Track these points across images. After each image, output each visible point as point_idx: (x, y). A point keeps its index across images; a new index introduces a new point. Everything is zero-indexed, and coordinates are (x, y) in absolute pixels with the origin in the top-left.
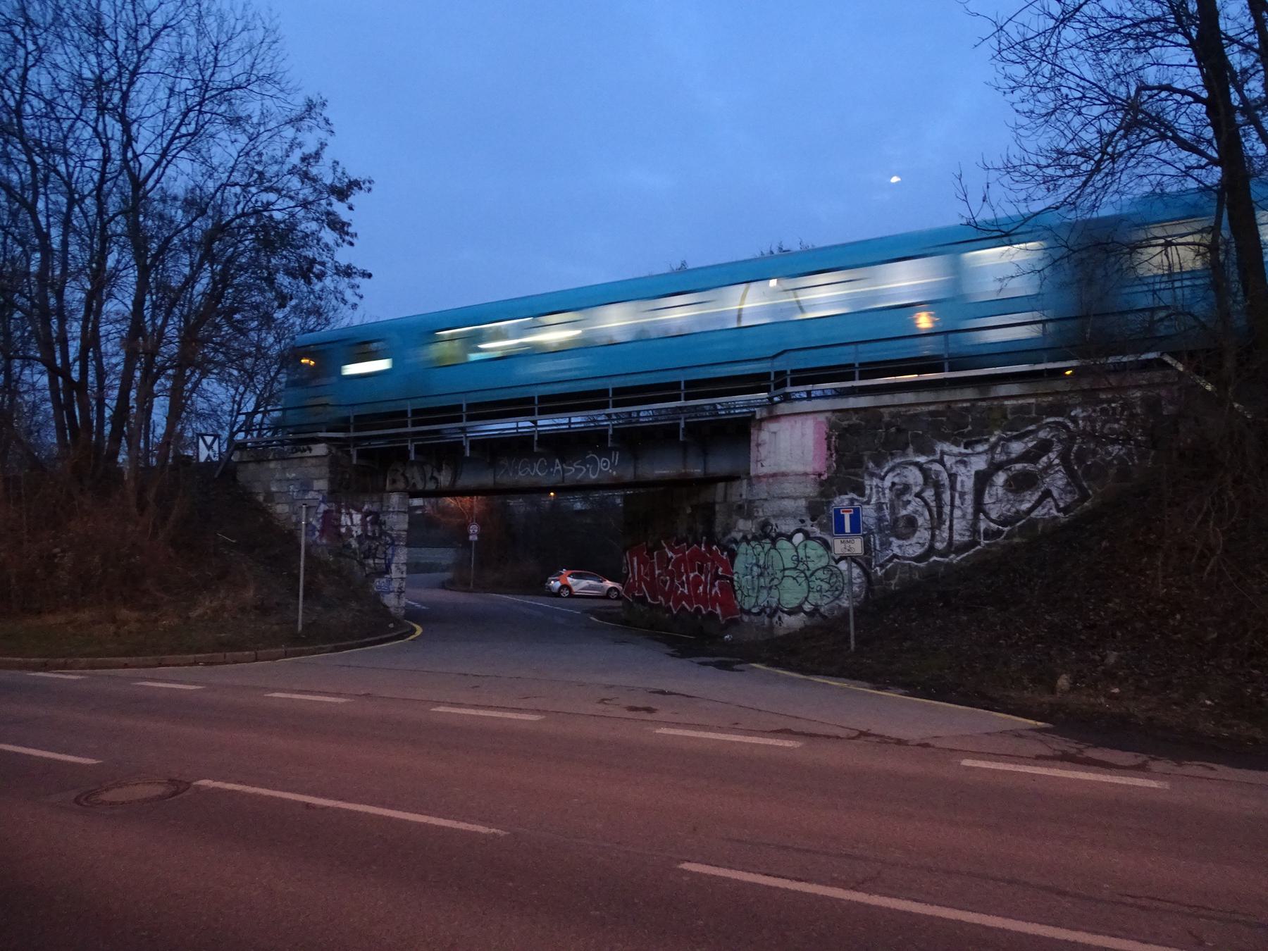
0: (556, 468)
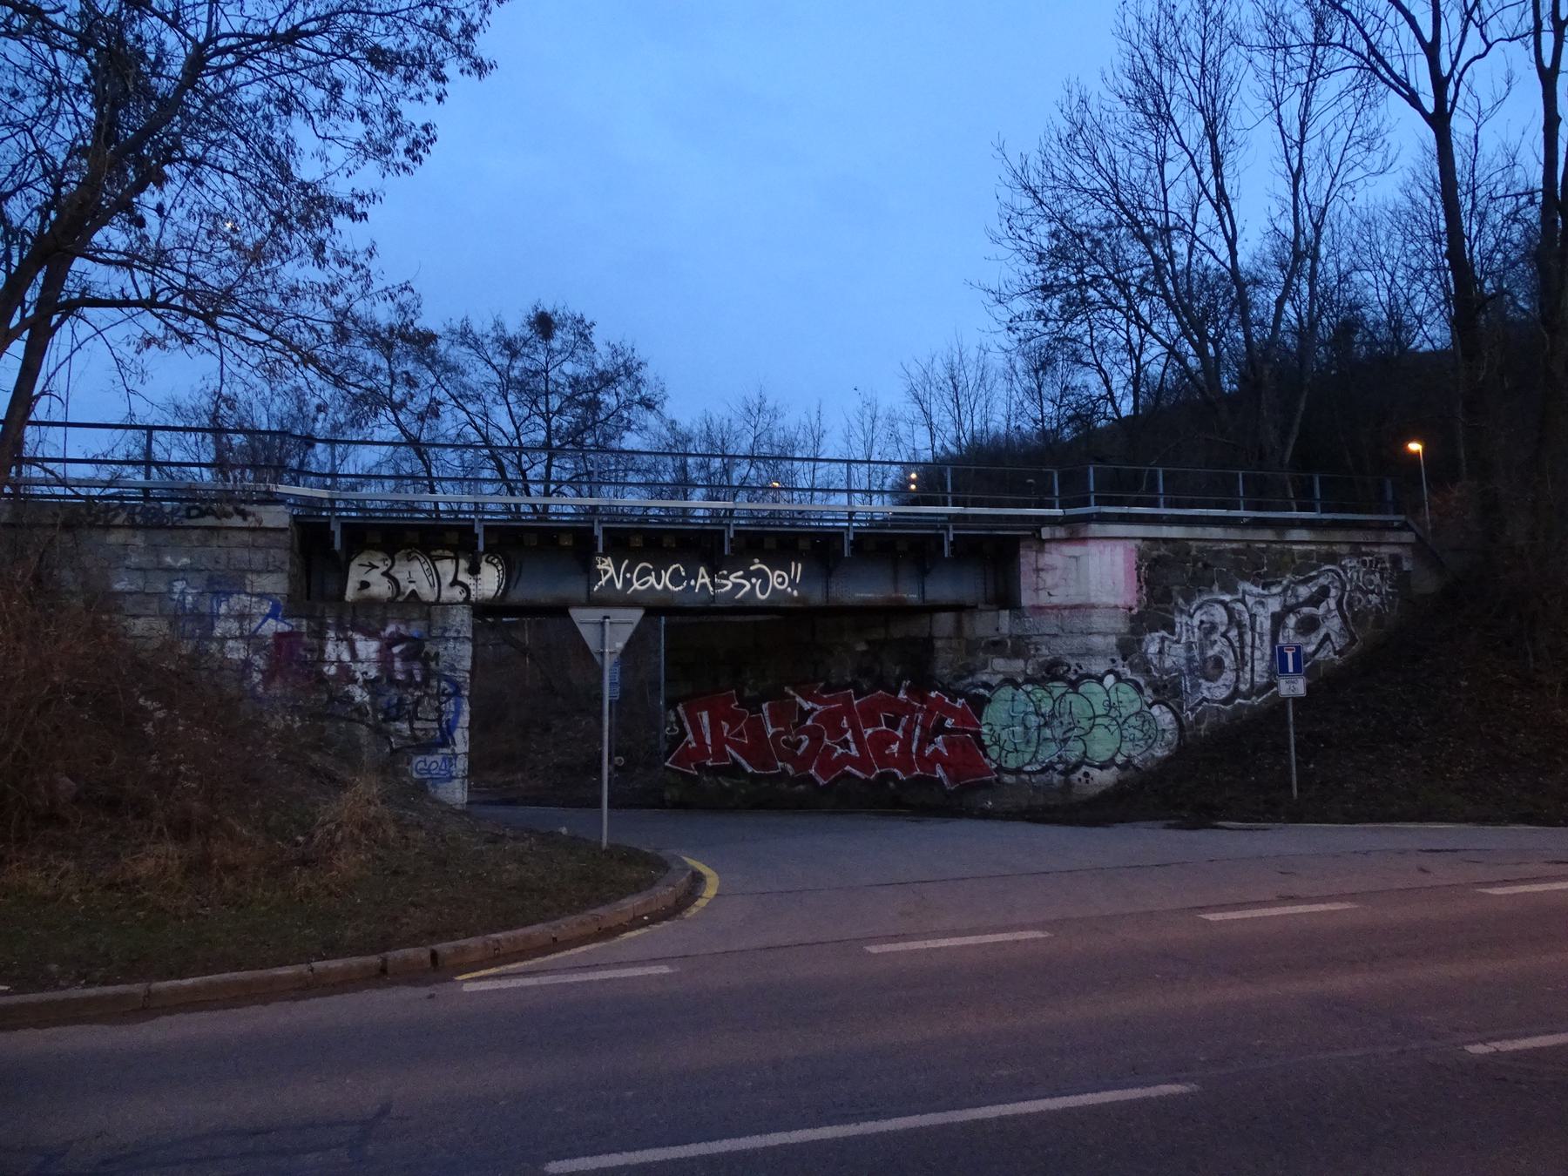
0: (700, 581)
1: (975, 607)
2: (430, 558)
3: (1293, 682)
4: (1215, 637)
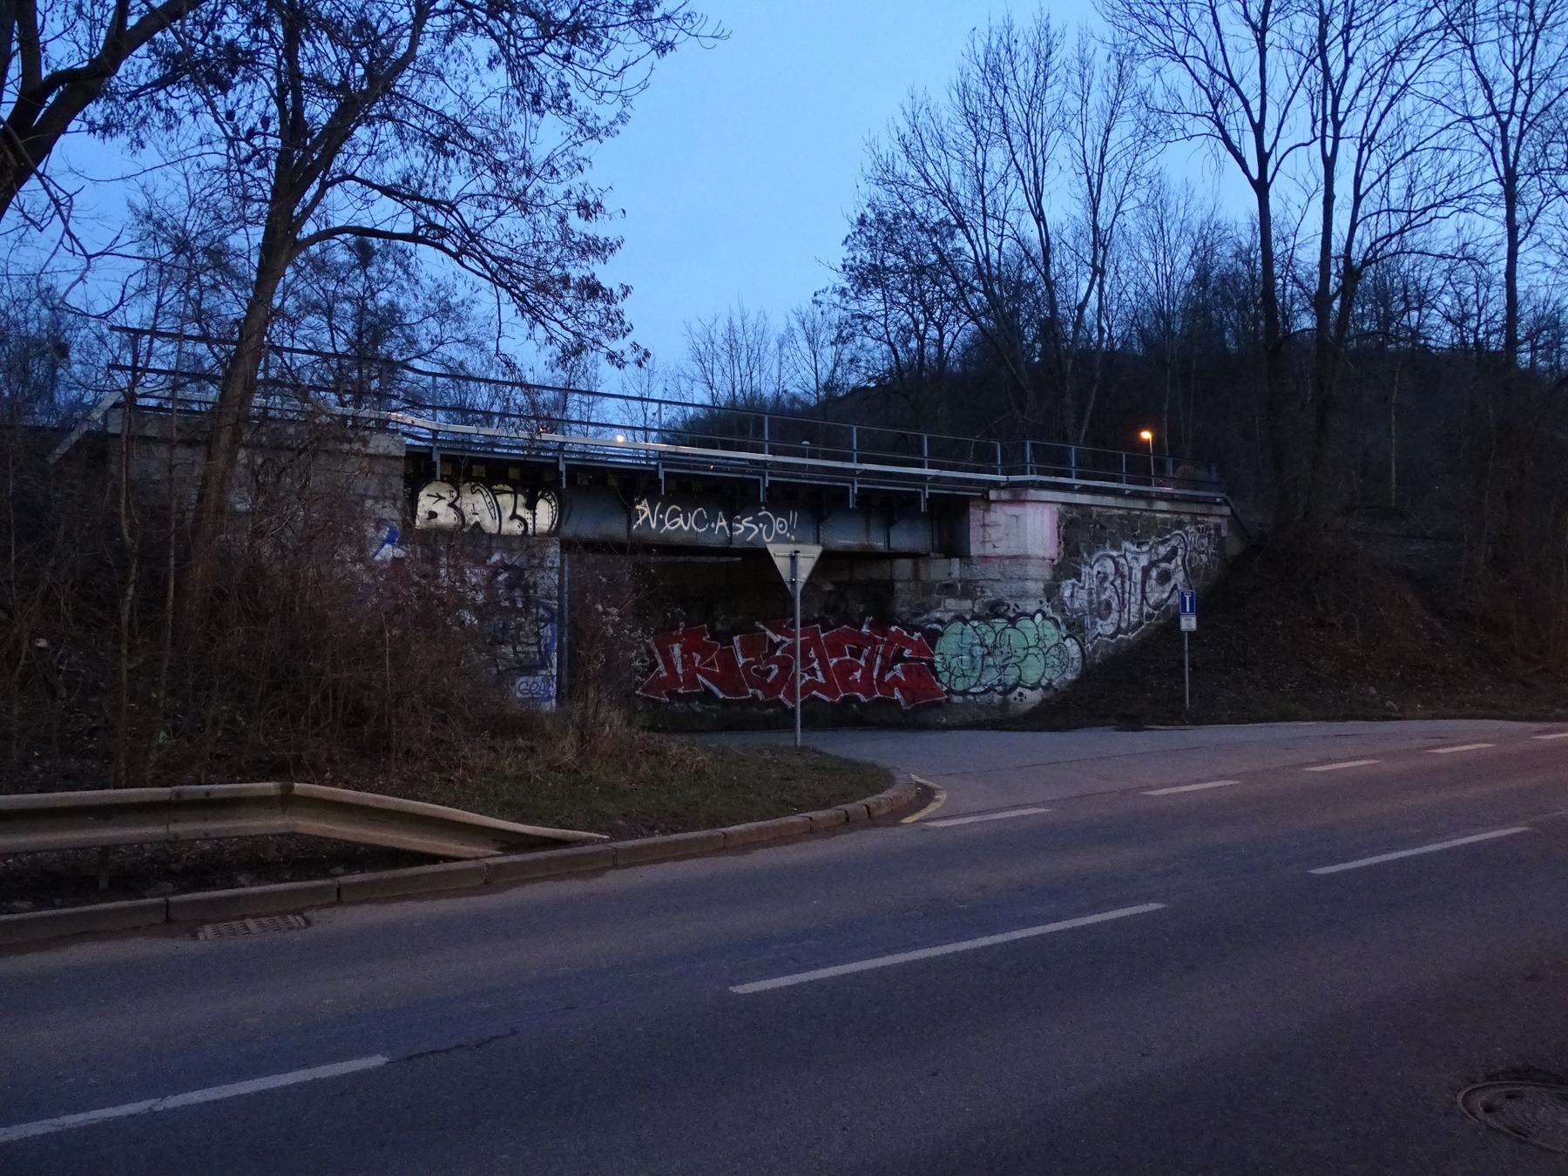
0: (719, 524)
1: (928, 555)
2: (492, 491)
4: (1107, 584)
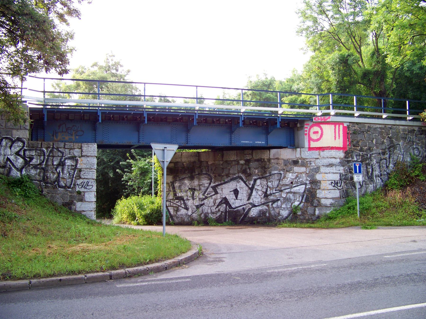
3: (358, 176)
